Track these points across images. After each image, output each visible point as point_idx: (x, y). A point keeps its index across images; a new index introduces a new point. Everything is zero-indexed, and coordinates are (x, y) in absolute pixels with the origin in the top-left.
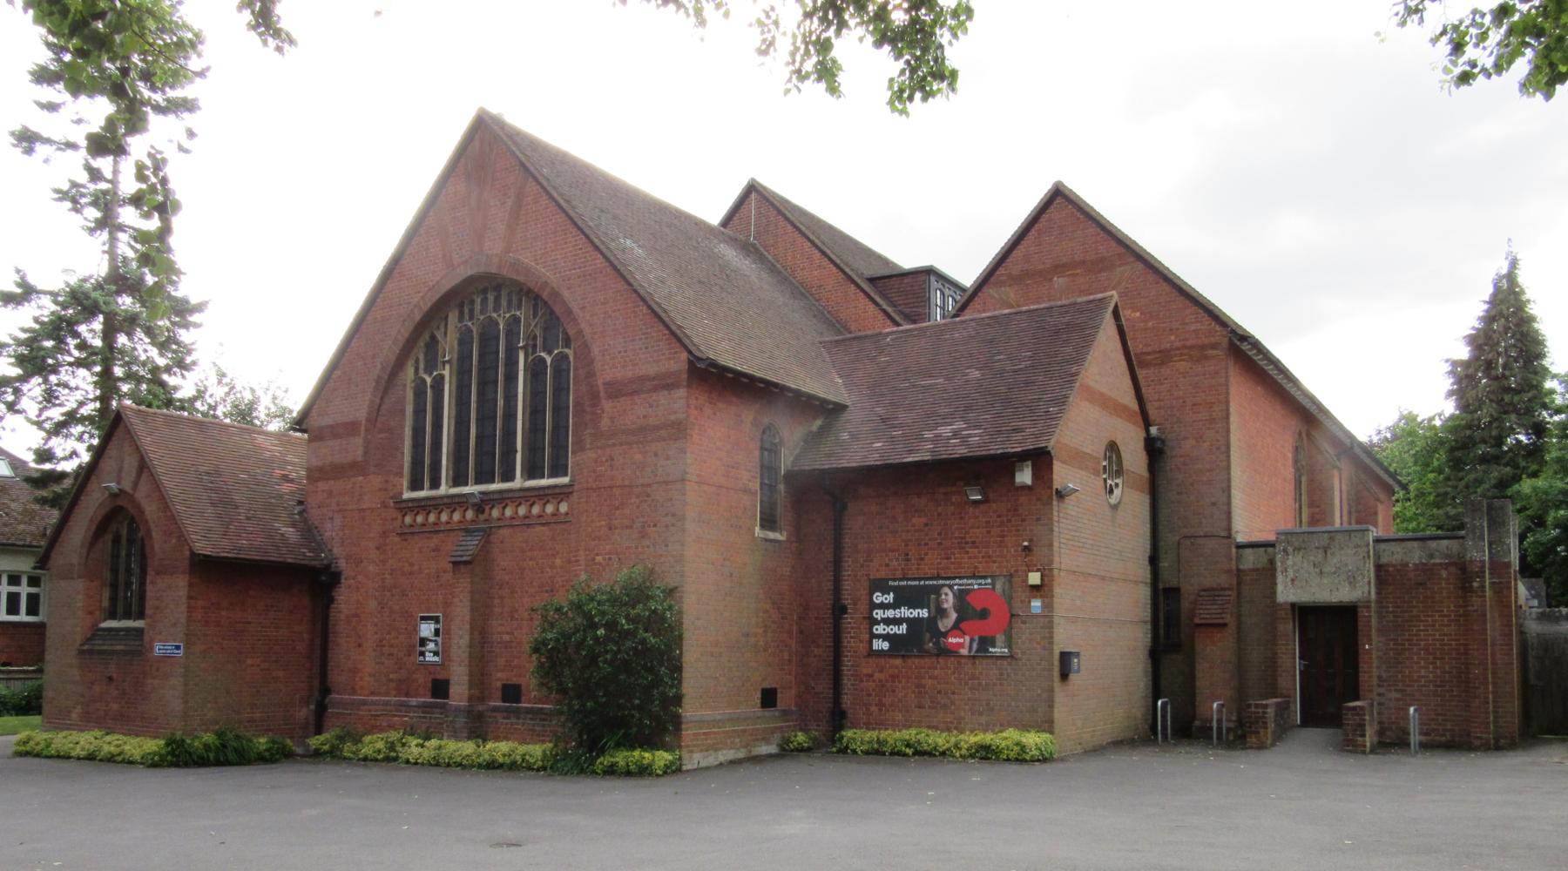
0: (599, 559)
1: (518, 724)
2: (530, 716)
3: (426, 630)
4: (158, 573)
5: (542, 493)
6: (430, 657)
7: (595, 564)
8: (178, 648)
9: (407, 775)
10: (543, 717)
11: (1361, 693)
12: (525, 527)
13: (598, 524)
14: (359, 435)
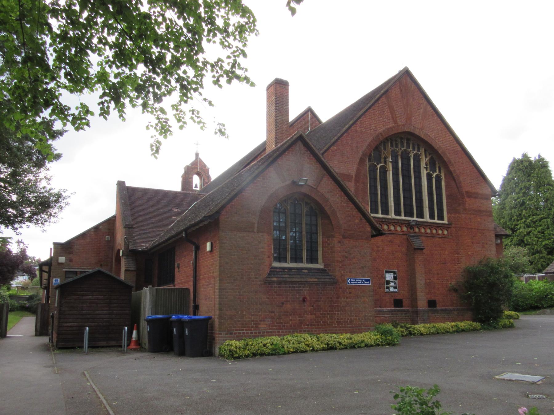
0: (469, 253)
1: (438, 316)
2: (443, 312)
3: (389, 277)
4: (344, 237)
5: (439, 225)
6: (392, 289)
7: (469, 255)
9: (423, 338)
10: (448, 312)
11: (403, 305)
12: (432, 238)
13: (468, 241)
14: (351, 182)
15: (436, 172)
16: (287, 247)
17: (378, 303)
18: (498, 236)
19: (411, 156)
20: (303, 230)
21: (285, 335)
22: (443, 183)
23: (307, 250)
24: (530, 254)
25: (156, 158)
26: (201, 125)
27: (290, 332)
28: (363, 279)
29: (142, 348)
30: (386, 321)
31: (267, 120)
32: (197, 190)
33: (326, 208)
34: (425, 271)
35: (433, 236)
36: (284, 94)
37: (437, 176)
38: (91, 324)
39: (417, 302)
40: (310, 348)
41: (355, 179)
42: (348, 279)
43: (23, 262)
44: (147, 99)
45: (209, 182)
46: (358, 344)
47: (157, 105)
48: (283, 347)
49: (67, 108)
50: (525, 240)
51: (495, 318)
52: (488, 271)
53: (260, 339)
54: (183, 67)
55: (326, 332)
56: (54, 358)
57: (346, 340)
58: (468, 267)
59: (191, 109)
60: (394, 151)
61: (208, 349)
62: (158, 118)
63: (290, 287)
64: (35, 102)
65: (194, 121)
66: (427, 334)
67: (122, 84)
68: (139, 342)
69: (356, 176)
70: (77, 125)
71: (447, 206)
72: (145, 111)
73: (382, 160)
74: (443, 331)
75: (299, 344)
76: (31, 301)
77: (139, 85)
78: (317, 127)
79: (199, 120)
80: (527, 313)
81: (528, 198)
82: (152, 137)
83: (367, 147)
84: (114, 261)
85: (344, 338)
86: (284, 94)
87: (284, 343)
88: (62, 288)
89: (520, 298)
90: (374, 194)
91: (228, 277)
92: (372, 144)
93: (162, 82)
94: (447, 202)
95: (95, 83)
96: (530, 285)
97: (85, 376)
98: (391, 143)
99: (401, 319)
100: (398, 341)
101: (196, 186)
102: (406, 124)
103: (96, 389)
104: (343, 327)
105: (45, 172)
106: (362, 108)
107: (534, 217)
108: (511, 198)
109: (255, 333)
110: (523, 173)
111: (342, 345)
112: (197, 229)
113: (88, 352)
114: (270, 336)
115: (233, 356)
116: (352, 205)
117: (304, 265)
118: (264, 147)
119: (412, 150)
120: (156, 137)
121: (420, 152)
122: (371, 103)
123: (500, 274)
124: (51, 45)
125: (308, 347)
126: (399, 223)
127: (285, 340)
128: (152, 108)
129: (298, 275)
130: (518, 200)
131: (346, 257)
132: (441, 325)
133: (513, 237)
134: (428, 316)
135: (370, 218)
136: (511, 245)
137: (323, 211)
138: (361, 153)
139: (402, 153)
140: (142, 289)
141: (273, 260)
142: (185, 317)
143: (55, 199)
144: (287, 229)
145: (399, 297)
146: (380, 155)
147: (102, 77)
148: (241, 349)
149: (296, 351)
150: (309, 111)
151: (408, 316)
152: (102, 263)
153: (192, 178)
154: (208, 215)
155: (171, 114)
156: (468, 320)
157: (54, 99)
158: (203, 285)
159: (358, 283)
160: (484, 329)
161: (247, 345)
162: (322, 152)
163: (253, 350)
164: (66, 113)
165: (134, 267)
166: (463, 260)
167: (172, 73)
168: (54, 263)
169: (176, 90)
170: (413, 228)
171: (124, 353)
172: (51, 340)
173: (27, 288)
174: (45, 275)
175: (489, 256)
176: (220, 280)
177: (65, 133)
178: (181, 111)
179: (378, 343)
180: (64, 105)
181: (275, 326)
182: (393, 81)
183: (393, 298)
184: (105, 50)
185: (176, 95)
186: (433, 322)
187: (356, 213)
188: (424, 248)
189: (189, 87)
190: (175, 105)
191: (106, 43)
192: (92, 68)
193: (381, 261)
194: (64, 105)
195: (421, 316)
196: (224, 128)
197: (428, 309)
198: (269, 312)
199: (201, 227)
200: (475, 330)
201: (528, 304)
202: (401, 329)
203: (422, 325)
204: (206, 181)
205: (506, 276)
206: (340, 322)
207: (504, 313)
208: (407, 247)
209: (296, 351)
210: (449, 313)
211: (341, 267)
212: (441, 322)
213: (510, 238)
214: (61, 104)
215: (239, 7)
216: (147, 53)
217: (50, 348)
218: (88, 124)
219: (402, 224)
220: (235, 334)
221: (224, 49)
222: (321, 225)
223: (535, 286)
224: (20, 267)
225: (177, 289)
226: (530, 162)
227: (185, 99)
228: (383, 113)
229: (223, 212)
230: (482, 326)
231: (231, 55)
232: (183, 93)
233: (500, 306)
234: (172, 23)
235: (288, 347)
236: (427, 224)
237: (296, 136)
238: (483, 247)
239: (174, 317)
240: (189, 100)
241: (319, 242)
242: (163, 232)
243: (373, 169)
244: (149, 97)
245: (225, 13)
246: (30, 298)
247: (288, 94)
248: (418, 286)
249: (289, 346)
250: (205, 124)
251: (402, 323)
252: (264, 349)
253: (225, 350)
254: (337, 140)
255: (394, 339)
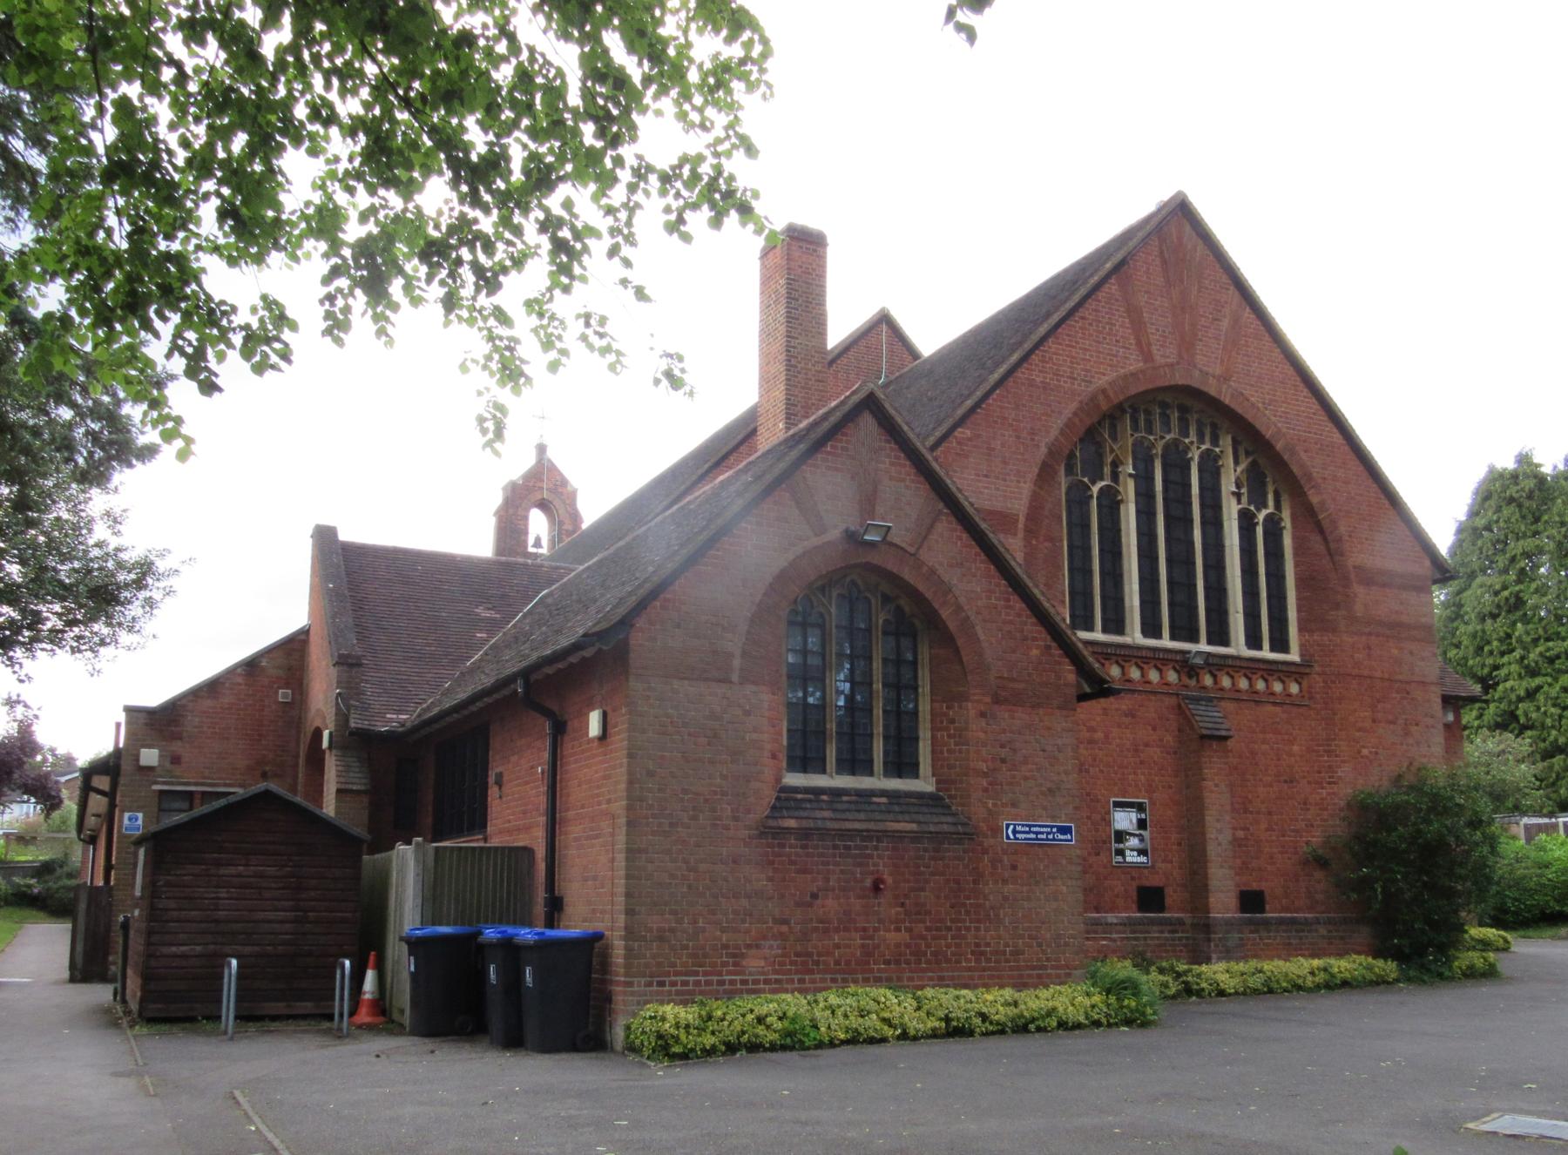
0: (1365, 752)
1: (1269, 938)
2: (1284, 927)
3: (1124, 820)
4: (997, 701)
6: (1132, 857)
8: (1065, 830)
9: (1225, 1005)
12: (1253, 704)
14: (1015, 534)
15: (1265, 506)
16: (828, 726)
17: (1095, 899)
18: (1453, 702)
19: (1192, 459)
20: (875, 678)
21: (821, 990)
22: (1287, 541)
23: (886, 738)
24: (1538, 757)
25: (497, 453)
26: (611, 358)
27: (834, 980)
28: (1052, 827)
29: (393, 1022)
30: (1114, 952)
31: (761, 350)
32: (542, 555)
33: (945, 613)
34: (1232, 804)
35: (1254, 698)
36: (814, 270)
37: (1269, 518)
38: (239, 948)
39: (1207, 898)
40: (895, 1028)
41: (1026, 526)
42: (1008, 826)
43: (24, 763)
44: (455, 282)
45: (574, 532)
46: (1038, 1019)
47: (483, 300)
48: (816, 1027)
49: (228, 308)
50: (1519, 712)
51: (1442, 949)
52: (1424, 807)
53: (746, 1003)
54: (564, 190)
55: (941, 982)
56: (135, 1049)
57: (1001, 1008)
58: (1362, 792)
59: (582, 311)
60: (1142, 443)
61: (591, 1028)
62: (491, 338)
63: (835, 847)
64: (133, 293)
65: (591, 347)
66: (1237, 993)
67: (388, 236)
68: (381, 1006)
69: (1029, 518)
70: (258, 358)
71: (1299, 610)
72: (452, 317)
73: (1107, 470)
74: (1284, 984)
75: (862, 1016)
76: (47, 878)
77: (431, 243)
78: (906, 370)
79: (604, 342)
80: (1531, 933)
81: (1534, 586)
82: (480, 393)
83: (1062, 432)
84: (301, 761)
85: (996, 1001)
86: (814, 270)
87: (818, 1014)
88: (160, 844)
89: (1510, 887)
90: (1080, 570)
91: (654, 816)
92: (1076, 420)
93: (496, 232)
94: (1299, 599)
95: (301, 237)
96: (1543, 849)
97: (238, 1103)
98: (1135, 422)
99: (1160, 945)
100: (1155, 1013)
101: (538, 544)
102: (1178, 363)
103: (276, 1143)
104: (990, 969)
105: (105, 497)
106: (1048, 315)
107: (1551, 644)
108: (1481, 586)
109: (732, 982)
110: (1520, 511)
111: (991, 1023)
112: (560, 670)
113: (235, 1033)
114: (774, 991)
115: (667, 1050)
116: (1019, 605)
117: (878, 782)
118: (752, 426)
119: (1195, 440)
120: (492, 393)
121: (1218, 446)
122: (1076, 298)
123: (1457, 815)
124: (172, 127)
125: (890, 1025)
126: (1154, 658)
127: (822, 1005)
128: (472, 309)
129: (859, 811)
130: (1506, 593)
131: (1003, 761)
132: (1278, 967)
133: (1484, 705)
134: (1241, 939)
135: (1074, 644)
136: (1480, 727)
137: (933, 621)
138: (1044, 450)
139: (1166, 448)
140: (392, 848)
141: (784, 764)
142: (526, 935)
143: (133, 576)
144: (828, 674)
145: (1155, 881)
146: (1100, 456)
147: (326, 222)
148: (691, 1030)
149: (854, 1040)
150: (884, 321)
151: (1180, 939)
152: (267, 768)
153: (526, 518)
154: (597, 629)
155: (524, 324)
156: (1359, 953)
157: (187, 283)
158: (577, 839)
159: (1037, 839)
160: (1409, 980)
161: (710, 1018)
162: (931, 440)
163: (728, 1032)
164: (224, 322)
165: (364, 781)
166: (1345, 771)
167: (528, 203)
168: (126, 766)
169: (539, 255)
170: (1197, 675)
171: (339, 1037)
172: (121, 995)
173: (35, 838)
174: (97, 803)
175: (1424, 760)
176: (629, 824)
177: (170, 384)
178: (553, 317)
179: (1096, 1017)
180: (217, 300)
181: (792, 963)
182: (1141, 235)
183: (1135, 884)
184: (327, 139)
185: (537, 273)
186: (1256, 956)
187: (1031, 627)
188: (1231, 733)
189: (578, 246)
190: (536, 301)
191: (331, 119)
192: (289, 191)
193: (1102, 771)
194: (217, 300)
195: (1220, 939)
196: (680, 366)
197: (1240, 919)
198: (774, 919)
199: (572, 665)
200: (1380, 983)
201: (1533, 906)
202: (1161, 977)
203: (1221, 966)
204: (568, 527)
205: (1476, 823)
206: (983, 953)
207: (1466, 932)
208: (1179, 730)
209: (854, 1040)
210: (1303, 931)
211: (986, 790)
212: (1279, 957)
213: (1477, 705)
214: (209, 298)
215: (720, 11)
216: (457, 148)
217: (121, 1018)
218: (286, 356)
219: (1165, 661)
220: (673, 984)
221: (687, 132)
222: (927, 661)
223: (1557, 854)
224: (16, 776)
225: (496, 849)
226: (1541, 480)
227: (564, 280)
228: (1111, 329)
229: (640, 623)
230: (1402, 969)
231: (707, 153)
232: (557, 265)
233: (1456, 912)
234: (532, 60)
235: (829, 1027)
236: (1238, 663)
237: (856, 399)
238: (1407, 734)
239: (490, 933)
240: (576, 284)
241: (920, 714)
242: (450, 679)
243: (1078, 498)
244: (460, 276)
245: (679, 26)
246: (45, 869)
247: (824, 272)
248: (1212, 850)
249: (834, 1023)
250: (623, 355)
251: (1162, 958)
252: (761, 1030)
253: (644, 1032)
254: (972, 410)
255: (1145, 1006)
